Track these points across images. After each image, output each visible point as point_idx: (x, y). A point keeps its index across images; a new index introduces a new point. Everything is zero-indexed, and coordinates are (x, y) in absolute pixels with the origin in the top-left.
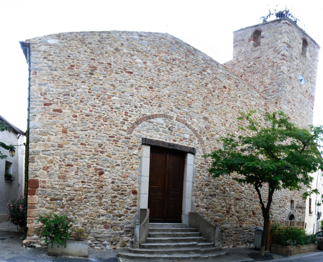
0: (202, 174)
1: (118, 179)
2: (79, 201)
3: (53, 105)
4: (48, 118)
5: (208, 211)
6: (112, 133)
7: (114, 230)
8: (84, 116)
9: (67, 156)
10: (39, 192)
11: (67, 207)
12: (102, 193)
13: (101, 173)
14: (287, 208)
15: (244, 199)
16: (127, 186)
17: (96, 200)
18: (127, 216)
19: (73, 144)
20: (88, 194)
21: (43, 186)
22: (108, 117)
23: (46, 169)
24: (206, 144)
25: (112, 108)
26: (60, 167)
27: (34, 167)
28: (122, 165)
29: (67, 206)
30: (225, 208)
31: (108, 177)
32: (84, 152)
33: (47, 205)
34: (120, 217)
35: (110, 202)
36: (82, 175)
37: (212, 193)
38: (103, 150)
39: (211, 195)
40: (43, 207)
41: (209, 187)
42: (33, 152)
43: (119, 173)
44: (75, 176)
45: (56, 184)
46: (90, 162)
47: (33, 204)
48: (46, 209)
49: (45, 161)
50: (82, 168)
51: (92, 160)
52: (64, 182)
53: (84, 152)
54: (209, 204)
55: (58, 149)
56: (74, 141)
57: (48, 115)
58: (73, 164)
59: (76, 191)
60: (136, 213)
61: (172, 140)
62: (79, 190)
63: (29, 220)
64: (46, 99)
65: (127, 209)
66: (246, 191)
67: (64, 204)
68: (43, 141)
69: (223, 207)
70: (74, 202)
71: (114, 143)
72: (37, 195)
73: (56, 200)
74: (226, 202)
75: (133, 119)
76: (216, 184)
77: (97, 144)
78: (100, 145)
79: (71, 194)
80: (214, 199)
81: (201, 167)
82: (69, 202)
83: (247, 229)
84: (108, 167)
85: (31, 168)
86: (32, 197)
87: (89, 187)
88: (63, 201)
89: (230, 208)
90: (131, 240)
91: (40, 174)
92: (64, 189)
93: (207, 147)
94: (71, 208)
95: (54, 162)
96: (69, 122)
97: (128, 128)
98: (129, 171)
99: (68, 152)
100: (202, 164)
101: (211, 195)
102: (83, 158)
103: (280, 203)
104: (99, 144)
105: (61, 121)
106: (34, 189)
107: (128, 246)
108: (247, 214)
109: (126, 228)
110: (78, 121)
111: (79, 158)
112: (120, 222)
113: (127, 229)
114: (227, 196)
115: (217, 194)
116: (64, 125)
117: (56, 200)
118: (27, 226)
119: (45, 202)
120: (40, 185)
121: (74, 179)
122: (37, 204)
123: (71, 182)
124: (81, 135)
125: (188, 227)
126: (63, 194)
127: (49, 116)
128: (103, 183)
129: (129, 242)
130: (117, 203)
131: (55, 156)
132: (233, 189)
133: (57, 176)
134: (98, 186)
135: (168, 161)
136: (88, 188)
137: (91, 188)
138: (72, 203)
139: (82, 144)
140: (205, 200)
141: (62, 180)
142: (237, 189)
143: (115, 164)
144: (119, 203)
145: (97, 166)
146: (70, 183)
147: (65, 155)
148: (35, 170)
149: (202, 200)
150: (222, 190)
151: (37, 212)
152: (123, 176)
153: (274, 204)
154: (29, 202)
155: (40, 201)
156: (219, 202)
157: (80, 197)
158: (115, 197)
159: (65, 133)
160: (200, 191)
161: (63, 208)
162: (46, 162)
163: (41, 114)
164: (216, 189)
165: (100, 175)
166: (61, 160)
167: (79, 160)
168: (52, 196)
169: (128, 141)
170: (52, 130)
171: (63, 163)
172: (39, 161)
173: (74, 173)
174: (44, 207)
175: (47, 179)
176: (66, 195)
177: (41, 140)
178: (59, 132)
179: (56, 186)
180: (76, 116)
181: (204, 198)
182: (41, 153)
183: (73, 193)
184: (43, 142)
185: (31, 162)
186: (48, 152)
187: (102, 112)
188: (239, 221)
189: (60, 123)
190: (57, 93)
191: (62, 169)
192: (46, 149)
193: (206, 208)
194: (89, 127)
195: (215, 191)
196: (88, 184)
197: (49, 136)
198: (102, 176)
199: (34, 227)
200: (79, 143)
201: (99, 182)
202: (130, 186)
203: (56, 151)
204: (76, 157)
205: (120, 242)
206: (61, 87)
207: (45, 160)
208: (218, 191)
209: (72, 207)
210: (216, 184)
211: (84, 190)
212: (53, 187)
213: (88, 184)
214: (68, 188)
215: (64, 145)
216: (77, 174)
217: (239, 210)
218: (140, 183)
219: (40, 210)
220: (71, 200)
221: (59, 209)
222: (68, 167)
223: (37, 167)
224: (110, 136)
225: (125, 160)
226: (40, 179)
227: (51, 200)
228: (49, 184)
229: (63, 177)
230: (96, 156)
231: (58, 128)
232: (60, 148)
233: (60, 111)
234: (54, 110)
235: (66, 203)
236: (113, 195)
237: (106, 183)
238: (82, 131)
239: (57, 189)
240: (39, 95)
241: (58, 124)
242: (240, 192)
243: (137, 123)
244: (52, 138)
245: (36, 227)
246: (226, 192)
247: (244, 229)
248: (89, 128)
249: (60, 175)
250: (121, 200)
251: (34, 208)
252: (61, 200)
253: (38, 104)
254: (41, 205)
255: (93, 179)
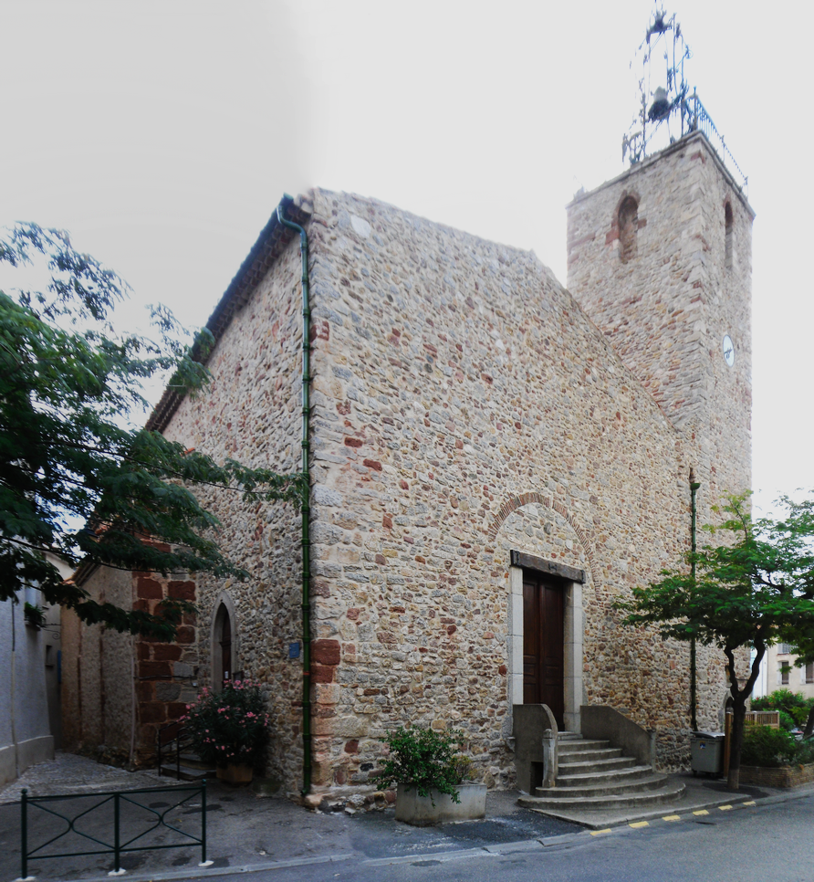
0: (594, 624)
1: (478, 643)
2: (418, 695)
3: (363, 446)
4: (355, 481)
5: (605, 701)
6: (466, 537)
7: (474, 753)
8: (419, 487)
9: (394, 587)
10: (342, 674)
11: (396, 709)
12: (453, 675)
13: (452, 630)
14: (720, 685)
15: (655, 672)
16: (492, 657)
17: (446, 691)
18: (493, 722)
19: (404, 558)
20: (431, 677)
21: (348, 660)
22: (458, 495)
23: (352, 615)
24: (596, 561)
25: (465, 475)
26: (380, 612)
27: (330, 610)
28: (484, 613)
29: (397, 706)
30: (628, 695)
31: (463, 639)
32: (423, 578)
33: (358, 706)
34: (481, 724)
35: (466, 692)
36: (421, 633)
37: (609, 664)
38: (454, 576)
39: (608, 669)
40: (350, 712)
41: (604, 652)
42: (325, 568)
43: (479, 630)
44: (408, 637)
45: (374, 655)
46: (433, 604)
47: (328, 704)
48: (355, 717)
49: (351, 595)
50: (421, 618)
51: (437, 600)
52: (389, 649)
53: (422, 580)
54: (607, 687)
55: (376, 567)
56: (405, 551)
57: (354, 472)
58: (404, 606)
59: (411, 670)
60: (506, 715)
61: (550, 555)
62: (416, 670)
63: (320, 743)
64: (350, 425)
65: (493, 706)
66: (658, 654)
67: (391, 701)
68: (345, 543)
69: (625, 692)
70: (409, 696)
71: (470, 559)
72: (337, 682)
73: (376, 692)
74: (629, 681)
75: (496, 505)
76: (614, 644)
77: (442, 562)
78: (448, 565)
79: (402, 679)
80: (613, 676)
81: (592, 610)
82: (400, 698)
83: (664, 736)
84: (463, 616)
85: (323, 612)
86: (327, 686)
87: (433, 661)
88: (389, 696)
89: (635, 694)
90: (501, 771)
91: (342, 628)
92: (389, 666)
93: (598, 566)
94: (402, 711)
95: (370, 600)
96: (396, 501)
97: (490, 526)
98: (494, 624)
99: (396, 576)
100: (592, 603)
101: (608, 669)
102: (420, 593)
103: (708, 674)
104: (447, 562)
105: (381, 495)
106: (330, 667)
107: (498, 785)
108: (661, 703)
109: (493, 747)
110: (410, 500)
111: (413, 593)
112: (484, 735)
113: (494, 750)
114: (630, 669)
115: (616, 665)
116: (386, 507)
117: (376, 692)
118: (318, 760)
119: (354, 699)
120: (342, 656)
121: (408, 644)
122: (338, 704)
123: (402, 649)
124: (416, 536)
125: (578, 739)
126: (388, 678)
127: (357, 478)
128: (456, 652)
129: (499, 776)
130: (478, 696)
131: (372, 586)
132: (639, 653)
133: (375, 634)
134: (448, 658)
135: (547, 590)
136: (432, 664)
137: (437, 665)
138: (406, 700)
139: (419, 559)
140: (600, 679)
141: (386, 645)
142: (645, 652)
143: (473, 609)
144: (482, 694)
145: (445, 613)
146: (400, 652)
147: (390, 583)
148: (331, 618)
149: (595, 679)
150: (623, 656)
151: (338, 725)
152: (486, 636)
153: (700, 678)
154: (320, 699)
155: (343, 698)
156: (620, 682)
157: (418, 686)
158: (475, 681)
159: (389, 527)
160: (593, 662)
161: (389, 712)
162: (354, 599)
163: (341, 467)
164: (614, 656)
165: (450, 633)
166: (383, 595)
167: (415, 598)
168: (368, 684)
169: (491, 558)
170: (364, 516)
171: (385, 603)
172: (338, 594)
173: (406, 627)
174: (353, 712)
175: (355, 642)
176: (394, 680)
177: (342, 538)
178: (378, 524)
179: (375, 659)
180: (405, 487)
181: (597, 677)
182: (342, 573)
183: (406, 677)
184: (345, 546)
185: (322, 595)
186: (358, 572)
187: (449, 482)
188: (650, 718)
189: (378, 500)
190: (371, 411)
191: (384, 617)
192: (354, 565)
193: (602, 696)
194: (429, 518)
195: (613, 660)
196: (431, 655)
197: (357, 530)
198: (454, 635)
199: (331, 764)
200: (414, 557)
201: (450, 651)
202: (496, 656)
203: (372, 571)
204: (408, 591)
205: (484, 778)
206: (378, 394)
207: (353, 593)
208: (617, 659)
209: (405, 709)
210: (614, 644)
211: (425, 669)
212: (369, 661)
213: (431, 655)
214: (397, 665)
215: (388, 558)
216: (413, 632)
217: (650, 695)
218: (510, 650)
219: (345, 719)
220: (402, 693)
221: (381, 715)
222: (396, 614)
223: (336, 610)
224: (463, 542)
225: (487, 601)
226: (343, 642)
227: (366, 694)
228: (360, 654)
229: (387, 639)
230: (443, 591)
231: (375, 512)
232: (379, 566)
233: (376, 466)
234: (368, 463)
235: (394, 699)
236: (471, 677)
237: (461, 652)
238: (418, 526)
239: (377, 667)
240: (335, 408)
241: (375, 502)
242: (648, 658)
243: (503, 515)
244: (365, 536)
245: (337, 765)
246: (630, 661)
247: (660, 735)
248: (429, 522)
249: (382, 631)
250: (483, 688)
251: (331, 714)
252: (384, 693)
253: (333, 436)
254: (345, 706)
255: (439, 642)
